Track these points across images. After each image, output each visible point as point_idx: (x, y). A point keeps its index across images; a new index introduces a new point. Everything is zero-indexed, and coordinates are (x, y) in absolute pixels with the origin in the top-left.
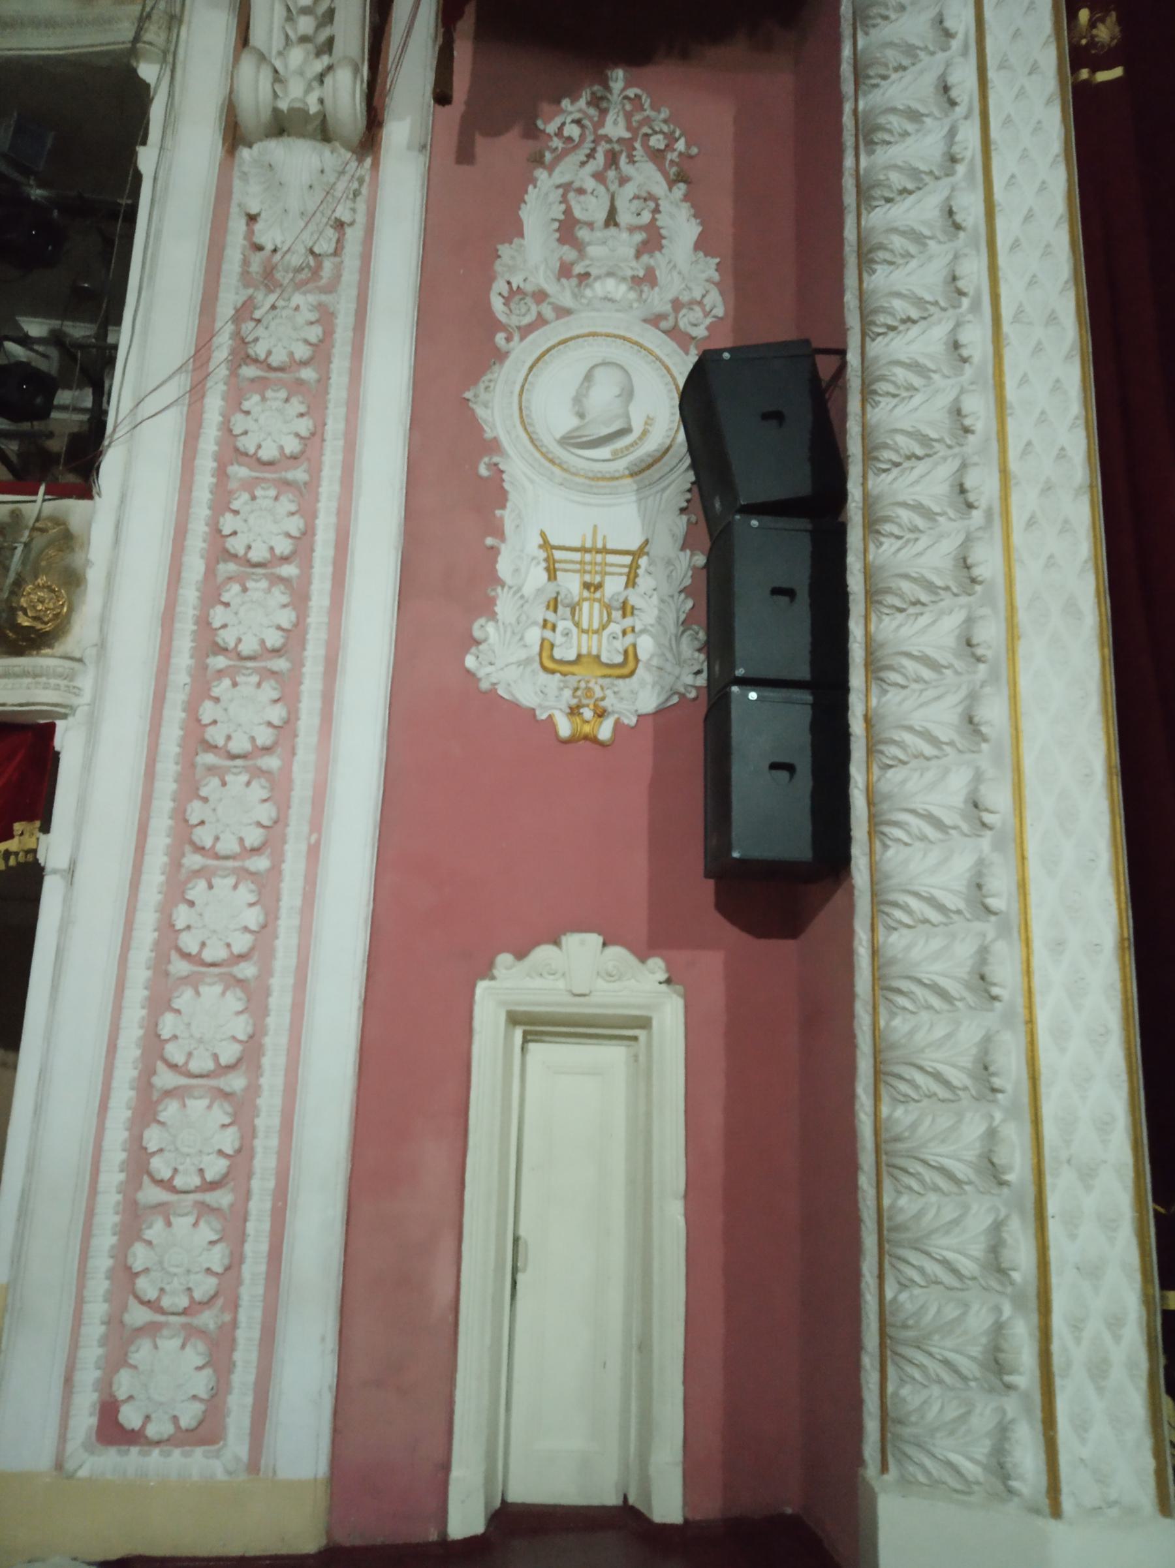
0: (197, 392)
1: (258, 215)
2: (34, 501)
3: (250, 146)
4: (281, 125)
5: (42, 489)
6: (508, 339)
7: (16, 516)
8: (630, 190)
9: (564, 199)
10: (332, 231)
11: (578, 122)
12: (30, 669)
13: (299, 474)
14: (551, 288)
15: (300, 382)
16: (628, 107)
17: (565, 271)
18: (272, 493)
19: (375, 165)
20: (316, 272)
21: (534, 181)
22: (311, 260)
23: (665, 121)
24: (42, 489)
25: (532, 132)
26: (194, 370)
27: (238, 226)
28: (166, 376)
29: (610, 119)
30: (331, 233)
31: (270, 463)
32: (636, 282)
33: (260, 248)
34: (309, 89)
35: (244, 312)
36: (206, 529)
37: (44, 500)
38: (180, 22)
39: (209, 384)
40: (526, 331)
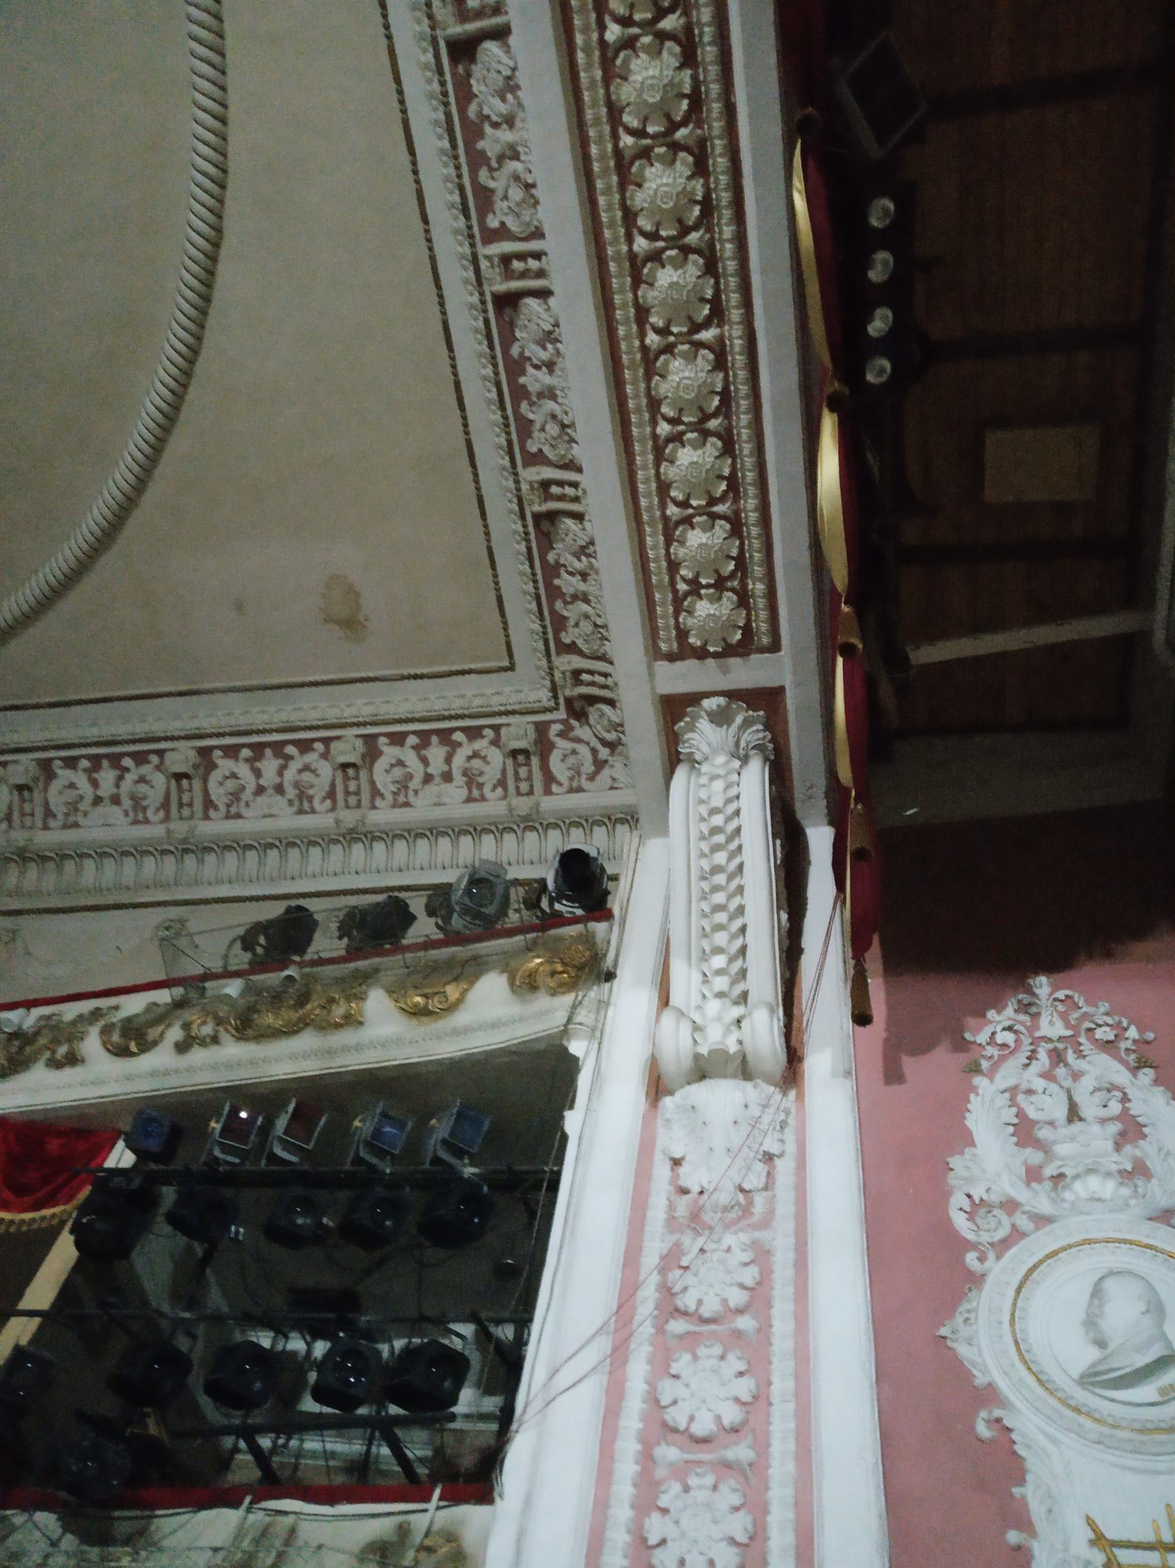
0: (619, 1356)
1: (683, 1158)
2: (425, 1511)
3: (671, 1093)
6: (982, 1259)
8: (1087, 1082)
9: (1013, 1102)
10: (761, 1165)
11: (1009, 1029)
13: (741, 1452)
14: (1021, 1194)
15: (738, 1334)
16: (1061, 1008)
17: (1033, 1175)
19: (800, 1097)
20: (747, 1210)
21: (974, 1089)
22: (741, 1197)
23: (1107, 1014)
24: (437, 1492)
25: (962, 1045)
26: (616, 1331)
27: (662, 1172)
29: (1044, 1021)
30: (760, 1168)
32: (1125, 1176)
33: (685, 1191)
35: (671, 1260)
37: (438, 1508)
38: (608, 1004)
40: (1002, 1247)
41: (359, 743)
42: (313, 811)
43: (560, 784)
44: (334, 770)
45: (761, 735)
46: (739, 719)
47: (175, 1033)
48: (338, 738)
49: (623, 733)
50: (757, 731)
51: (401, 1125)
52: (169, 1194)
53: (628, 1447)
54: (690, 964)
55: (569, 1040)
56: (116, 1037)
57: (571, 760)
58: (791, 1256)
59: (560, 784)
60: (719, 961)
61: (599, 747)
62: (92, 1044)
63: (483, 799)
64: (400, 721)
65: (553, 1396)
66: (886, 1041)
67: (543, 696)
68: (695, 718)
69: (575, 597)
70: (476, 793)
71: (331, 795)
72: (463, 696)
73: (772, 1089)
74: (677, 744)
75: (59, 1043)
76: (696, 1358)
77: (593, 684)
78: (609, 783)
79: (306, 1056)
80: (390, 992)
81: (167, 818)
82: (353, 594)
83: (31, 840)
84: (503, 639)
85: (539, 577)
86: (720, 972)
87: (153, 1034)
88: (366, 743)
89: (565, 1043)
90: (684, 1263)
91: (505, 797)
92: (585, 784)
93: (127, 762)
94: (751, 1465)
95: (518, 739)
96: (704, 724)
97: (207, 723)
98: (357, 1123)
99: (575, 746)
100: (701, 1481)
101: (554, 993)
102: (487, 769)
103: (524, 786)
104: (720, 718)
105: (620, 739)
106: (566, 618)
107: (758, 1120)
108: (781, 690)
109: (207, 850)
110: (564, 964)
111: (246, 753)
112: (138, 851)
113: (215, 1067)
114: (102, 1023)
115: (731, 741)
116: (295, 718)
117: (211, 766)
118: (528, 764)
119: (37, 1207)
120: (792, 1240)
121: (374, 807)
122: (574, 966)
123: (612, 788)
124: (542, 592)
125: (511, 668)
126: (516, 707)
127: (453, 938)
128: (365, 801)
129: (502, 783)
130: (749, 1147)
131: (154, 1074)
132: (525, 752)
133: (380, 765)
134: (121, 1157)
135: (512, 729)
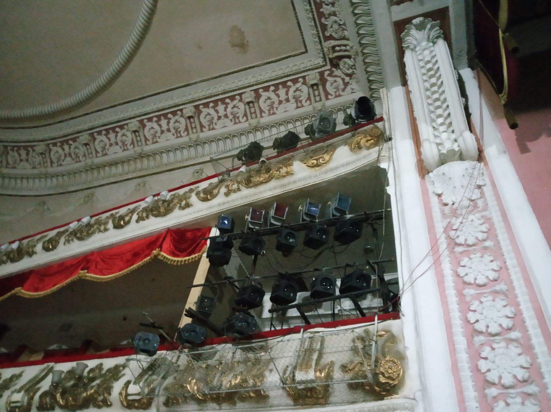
0: (437, 263)
1: (442, 194)
2: (374, 324)
3: (432, 172)
4: (443, 160)
5: (376, 318)
7: (367, 332)
10: (477, 190)
12: (391, 406)
13: (501, 286)
15: (486, 248)
18: (490, 298)
19: (486, 164)
20: (476, 206)
22: (472, 203)
24: (376, 318)
26: (433, 255)
27: (434, 200)
28: (177, 171)
30: (477, 191)
31: (484, 285)
33: (446, 205)
34: (453, 144)
35: (448, 228)
36: (461, 322)
37: (378, 323)
38: (392, 149)
39: (442, 258)
41: (253, 92)
42: (240, 122)
43: (332, 95)
44: (245, 105)
45: (438, 32)
46: (429, 26)
47: (223, 190)
48: (244, 93)
49: (355, 69)
50: (437, 30)
51: (317, 207)
52: (237, 243)
53: (451, 293)
54: (427, 124)
55: (380, 163)
56: (202, 195)
57: (335, 85)
58: (500, 218)
59: (332, 95)
60: (440, 120)
61: (345, 77)
62: (194, 199)
63: (303, 106)
64: (266, 82)
65: (414, 280)
66: (517, 140)
67: (320, 61)
68: (409, 30)
69: (330, 15)
70: (299, 105)
71: (245, 115)
72: (288, 67)
73: (475, 162)
74: (401, 43)
75: (182, 201)
76: (470, 259)
77: (340, 51)
78: (351, 91)
79: (275, 188)
80: (302, 161)
81: (188, 134)
82: (241, 33)
83: (142, 150)
84: (301, 40)
85: (314, 10)
86: (442, 124)
87: (215, 191)
88: (255, 93)
89: (379, 165)
90: (454, 228)
91: (311, 104)
92: (341, 93)
93: (170, 116)
94: (507, 290)
95: (313, 80)
96: (414, 32)
97: (196, 96)
98: (300, 208)
99: (335, 79)
100: (487, 300)
101: (368, 148)
102: (302, 94)
103: (318, 99)
104: (420, 27)
105: (353, 72)
106: (327, 25)
107: (472, 174)
108: (447, 8)
109: (205, 143)
110: (371, 136)
111: (211, 105)
112: (180, 148)
113: (241, 198)
114: (195, 192)
115: (426, 36)
116: (227, 88)
117: (200, 112)
118: (318, 89)
119: (189, 255)
120: (499, 213)
121: (262, 117)
122: (376, 137)
123: (352, 93)
124: (316, 16)
125: (306, 51)
126: (310, 68)
127: (315, 142)
128: (259, 115)
129: (309, 98)
130: (471, 184)
131: (219, 205)
132: (316, 85)
133: (262, 100)
134: (215, 232)
135: (311, 77)
